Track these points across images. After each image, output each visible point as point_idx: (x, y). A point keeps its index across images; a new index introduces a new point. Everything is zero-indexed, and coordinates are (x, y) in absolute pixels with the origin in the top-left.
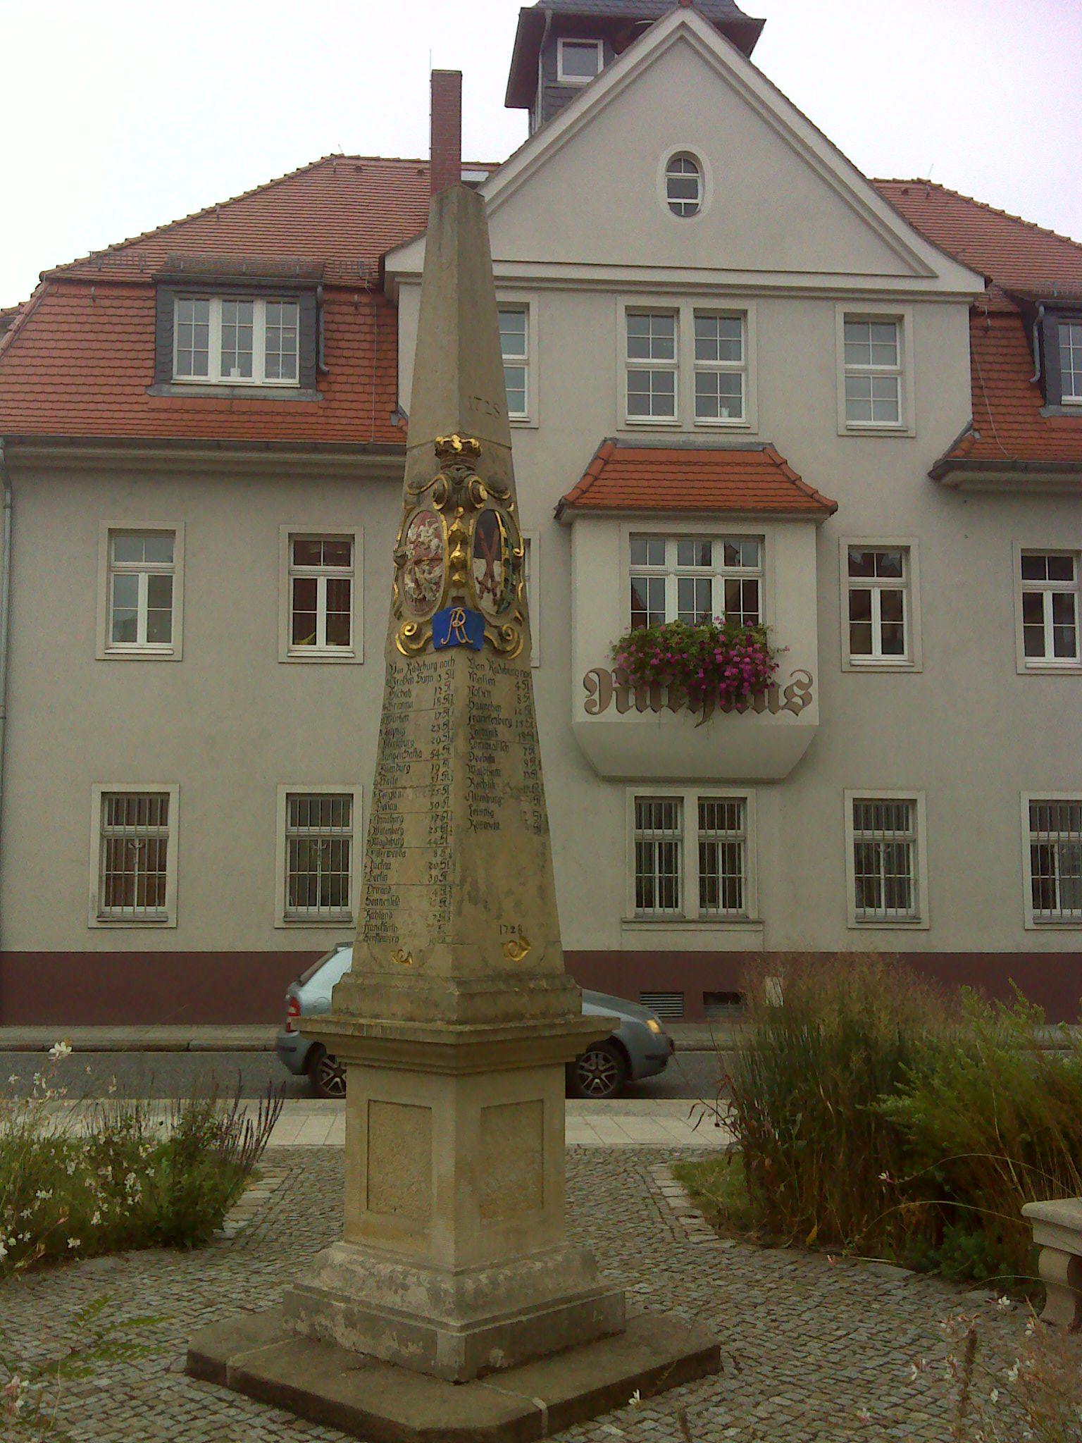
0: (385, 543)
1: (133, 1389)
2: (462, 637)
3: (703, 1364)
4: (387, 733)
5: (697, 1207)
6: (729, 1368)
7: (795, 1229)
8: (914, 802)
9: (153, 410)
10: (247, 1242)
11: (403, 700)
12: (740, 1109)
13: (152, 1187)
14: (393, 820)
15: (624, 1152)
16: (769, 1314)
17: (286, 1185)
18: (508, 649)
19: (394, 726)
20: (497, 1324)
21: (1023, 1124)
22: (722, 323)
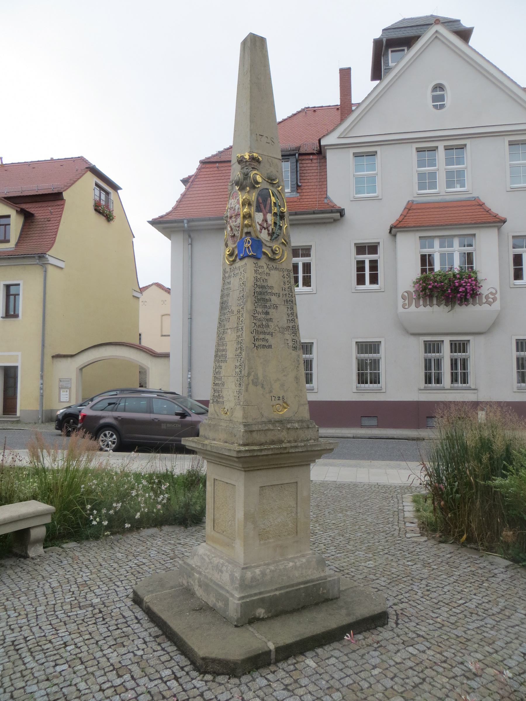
3: (378, 620)
6: (391, 623)
8: (380, 342)
16: (427, 586)
18: (277, 257)
19: (225, 299)
20: (261, 596)
22: (456, 149)
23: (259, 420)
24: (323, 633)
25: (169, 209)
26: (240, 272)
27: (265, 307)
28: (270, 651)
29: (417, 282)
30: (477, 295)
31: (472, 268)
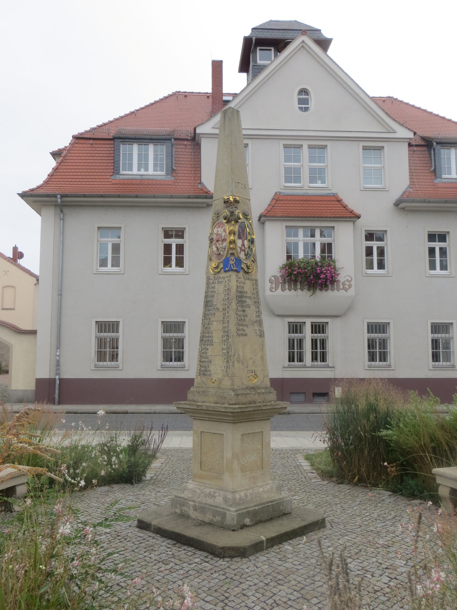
0: (199, 231)
1: (118, 533)
2: (234, 267)
3: (319, 525)
4: (207, 302)
5: (314, 469)
7: (350, 477)
8: (389, 323)
9: (113, 184)
10: (154, 482)
11: (213, 290)
12: (330, 435)
13: (120, 462)
14: (209, 333)
15: (287, 450)
17: (167, 462)
20: (247, 510)
21: (432, 441)
22: (319, 147)
23: (241, 387)
24: (291, 531)
25: (40, 182)
26: (224, 281)
27: (243, 306)
28: (263, 541)
29: (283, 268)
30: (336, 281)
31: (331, 257)
